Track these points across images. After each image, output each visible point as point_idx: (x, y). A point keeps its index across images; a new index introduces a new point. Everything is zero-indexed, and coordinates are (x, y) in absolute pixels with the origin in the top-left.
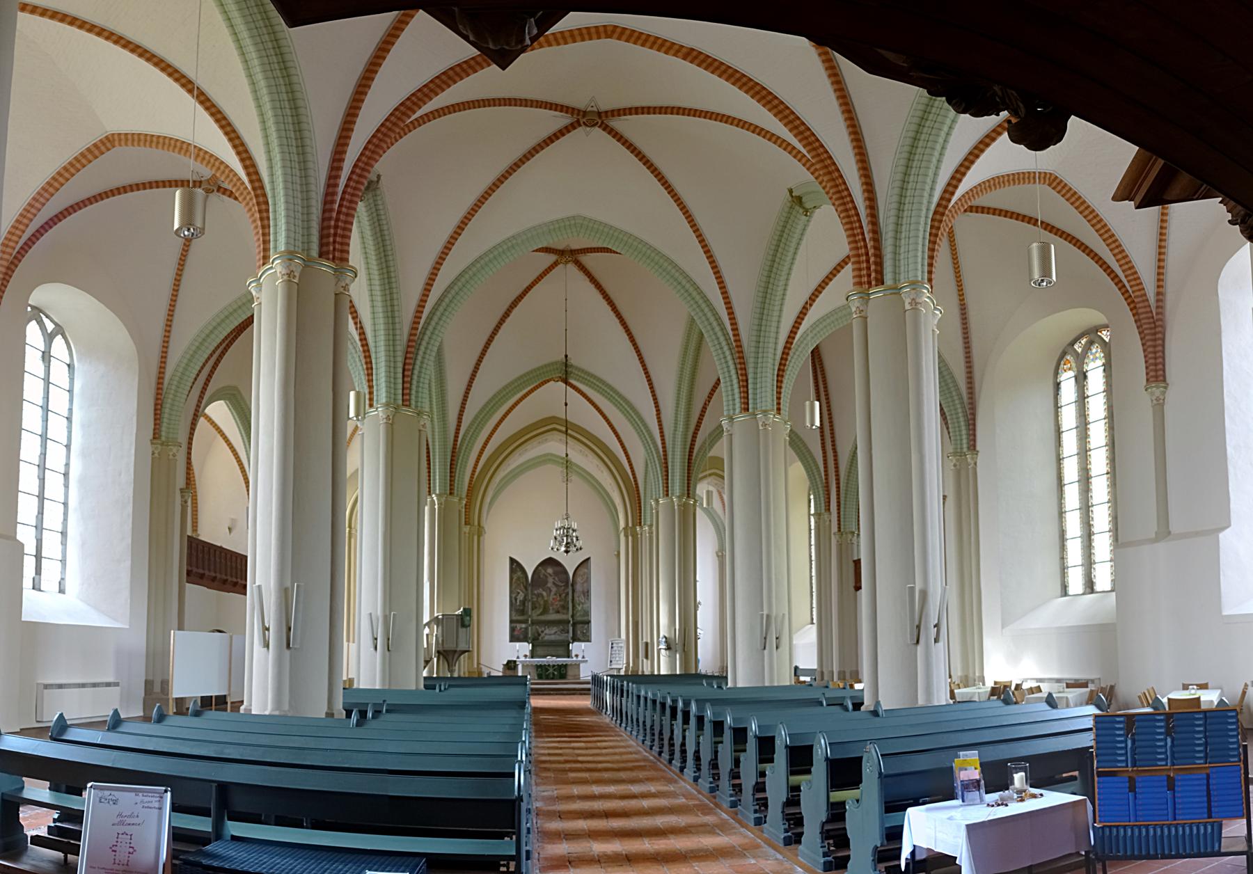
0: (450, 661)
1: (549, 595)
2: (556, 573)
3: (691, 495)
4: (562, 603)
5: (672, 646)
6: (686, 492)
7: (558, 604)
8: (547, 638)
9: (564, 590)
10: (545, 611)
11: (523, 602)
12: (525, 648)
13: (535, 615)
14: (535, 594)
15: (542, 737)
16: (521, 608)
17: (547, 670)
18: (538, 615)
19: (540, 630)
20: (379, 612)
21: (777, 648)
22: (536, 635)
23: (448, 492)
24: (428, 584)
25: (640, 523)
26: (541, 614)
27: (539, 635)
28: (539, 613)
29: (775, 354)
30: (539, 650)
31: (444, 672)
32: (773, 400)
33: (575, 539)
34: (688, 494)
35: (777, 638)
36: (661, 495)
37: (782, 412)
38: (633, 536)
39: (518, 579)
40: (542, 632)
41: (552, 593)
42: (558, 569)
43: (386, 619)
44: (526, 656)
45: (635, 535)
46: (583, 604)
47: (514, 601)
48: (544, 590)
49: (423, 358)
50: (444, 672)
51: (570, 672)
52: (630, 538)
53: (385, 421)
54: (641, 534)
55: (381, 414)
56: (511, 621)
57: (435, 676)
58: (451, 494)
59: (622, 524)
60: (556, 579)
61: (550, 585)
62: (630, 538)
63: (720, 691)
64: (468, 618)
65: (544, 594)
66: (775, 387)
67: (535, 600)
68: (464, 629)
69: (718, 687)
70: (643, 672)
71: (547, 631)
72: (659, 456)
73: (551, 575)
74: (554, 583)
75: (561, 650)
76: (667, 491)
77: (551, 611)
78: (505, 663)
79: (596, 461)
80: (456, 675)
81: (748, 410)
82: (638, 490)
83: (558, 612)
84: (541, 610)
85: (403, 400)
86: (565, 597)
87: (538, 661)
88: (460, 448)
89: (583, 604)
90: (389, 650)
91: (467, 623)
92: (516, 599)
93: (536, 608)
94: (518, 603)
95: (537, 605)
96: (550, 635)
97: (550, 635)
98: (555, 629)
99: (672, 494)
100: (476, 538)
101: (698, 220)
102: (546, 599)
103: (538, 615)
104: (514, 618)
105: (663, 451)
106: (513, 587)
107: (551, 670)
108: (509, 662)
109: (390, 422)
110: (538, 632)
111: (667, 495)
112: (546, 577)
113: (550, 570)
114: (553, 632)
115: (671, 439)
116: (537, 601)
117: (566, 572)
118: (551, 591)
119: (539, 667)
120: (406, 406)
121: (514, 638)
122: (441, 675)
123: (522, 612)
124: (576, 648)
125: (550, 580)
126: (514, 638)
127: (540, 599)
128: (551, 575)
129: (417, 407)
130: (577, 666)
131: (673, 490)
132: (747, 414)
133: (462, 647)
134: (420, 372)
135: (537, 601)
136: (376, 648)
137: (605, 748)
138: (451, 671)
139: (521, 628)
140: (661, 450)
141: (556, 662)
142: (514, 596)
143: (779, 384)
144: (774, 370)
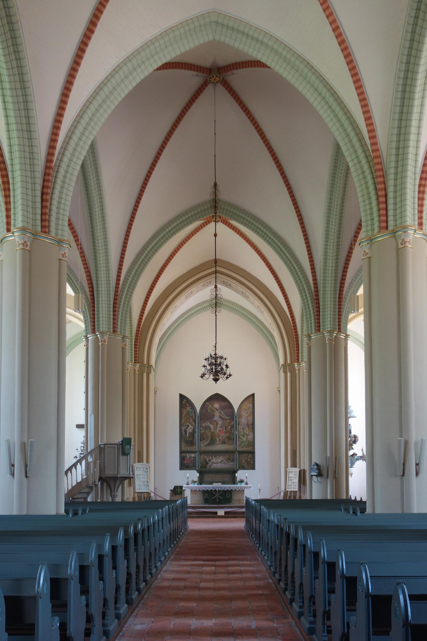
0: (113, 489)
1: (215, 428)
2: (222, 408)
3: (342, 330)
4: (227, 435)
5: (324, 472)
6: (337, 327)
7: (224, 435)
8: (214, 466)
9: (229, 423)
10: (212, 441)
11: (193, 434)
12: (194, 475)
13: (203, 446)
14: (203, 427)
15: (180, 560)
16: (191, 439)
17: (214, 495)
18: (206, 446)
19: (208, 459)
20: (16, 440)
21: (417, 474)
22: (204, 463)
23: (112, 330)
24: (93, 416)
25: (298, 359)
26: (208, 445)
27: (207, 463)
28: (206, 443)
29: (416, 161)
30: (207, 477)
31: (107, 497)
32: (414, 215)
33: (224, 367)
34: (339, 329)
35: (417, 465)
36: (313, 331)
37: (424, 227)
38: (291, 372)
39: (188, 413)
40: (210, 461)
41: (219, 426)
42: (224, 404)
43: (23, 446)
44: (194, 482)
45: (293, 371)
46: (247, 435)
47: (184, 433)
48: (211, 423)
49: (64, 182)
50: (107, 497)
51: (235, 497)
52: (289, 374)
53: (21, 246)
54: (299, 370)
55: (17, 239)
56: (181, 452)
57: (99, 501)
58: (114, 332)
59: (282, 362)
60: (222, 413)
61: (216, 418)
62: (289, 374)
63: (355, 517)
64: (128, 447)
65: (212, 426)
66: (417, 199)
67: (203, 432)
68: (125, 457)
69: (353, 513)
70: (300, 496)
71: (214, 460)
72: (310, 293)
73: (218, 410)
74: (220, 417)
75: (227, 477)
76: (319, 327)
77: (217, 442)
78: (172, 489)
79: (257, 302)
80: (118, 499)
81: (387, 228)
82: (296, 329)
83: (224, 443)
84: (208, 442)
85: (42, 227)
86: (231, 429)
87: (205, 487)
88: (123, 288)
89: (247, 435)
90: (26, 476)
91: (126, 451)
92: (186, 432)
93: (204, 439)
94: (188, 435)
95: (205, 436)
96: (217, 463)
97: (217, 463)
98: (221, 459)
99: (324, 329)
100: (145, 375)
101: (367, 88)
102: (213, 431)
103: (206, 446)
104: (184, 449)
105: (315, 288)
106: (183, 421)
107: (217, 495)
108: (176, 487)
109: (28, 248)
110: (206, 461)
111: (319, 330)
112: (213, 411)
113: (217, 405)
114: (219, 460)
115: (322, 275)
116: (205, 433)
117: (230, 406)
118: (217, 423)
119: (205, 492)
120: (45, 232)
121: (184, 466)
122: (105, 500)
123: (191, 443)
124: (240, 474)
125: (217, 414)
126: (184, 466)
127: (207, 431)
128: (218, 410)
129: (57, 234)
130: (242, 491)
131: (324, 326)
132: (386, 232)
133: (123, 473)
134: (60, 198)
135: (205, 433)
136: (13, 475)
137: (233, 573)
138: (113, 497)
139: (190, 458)
140: (312, 286)
141: (222, 488)
142: (183, 428)
143: (421, 195)
144: (415, 179)
